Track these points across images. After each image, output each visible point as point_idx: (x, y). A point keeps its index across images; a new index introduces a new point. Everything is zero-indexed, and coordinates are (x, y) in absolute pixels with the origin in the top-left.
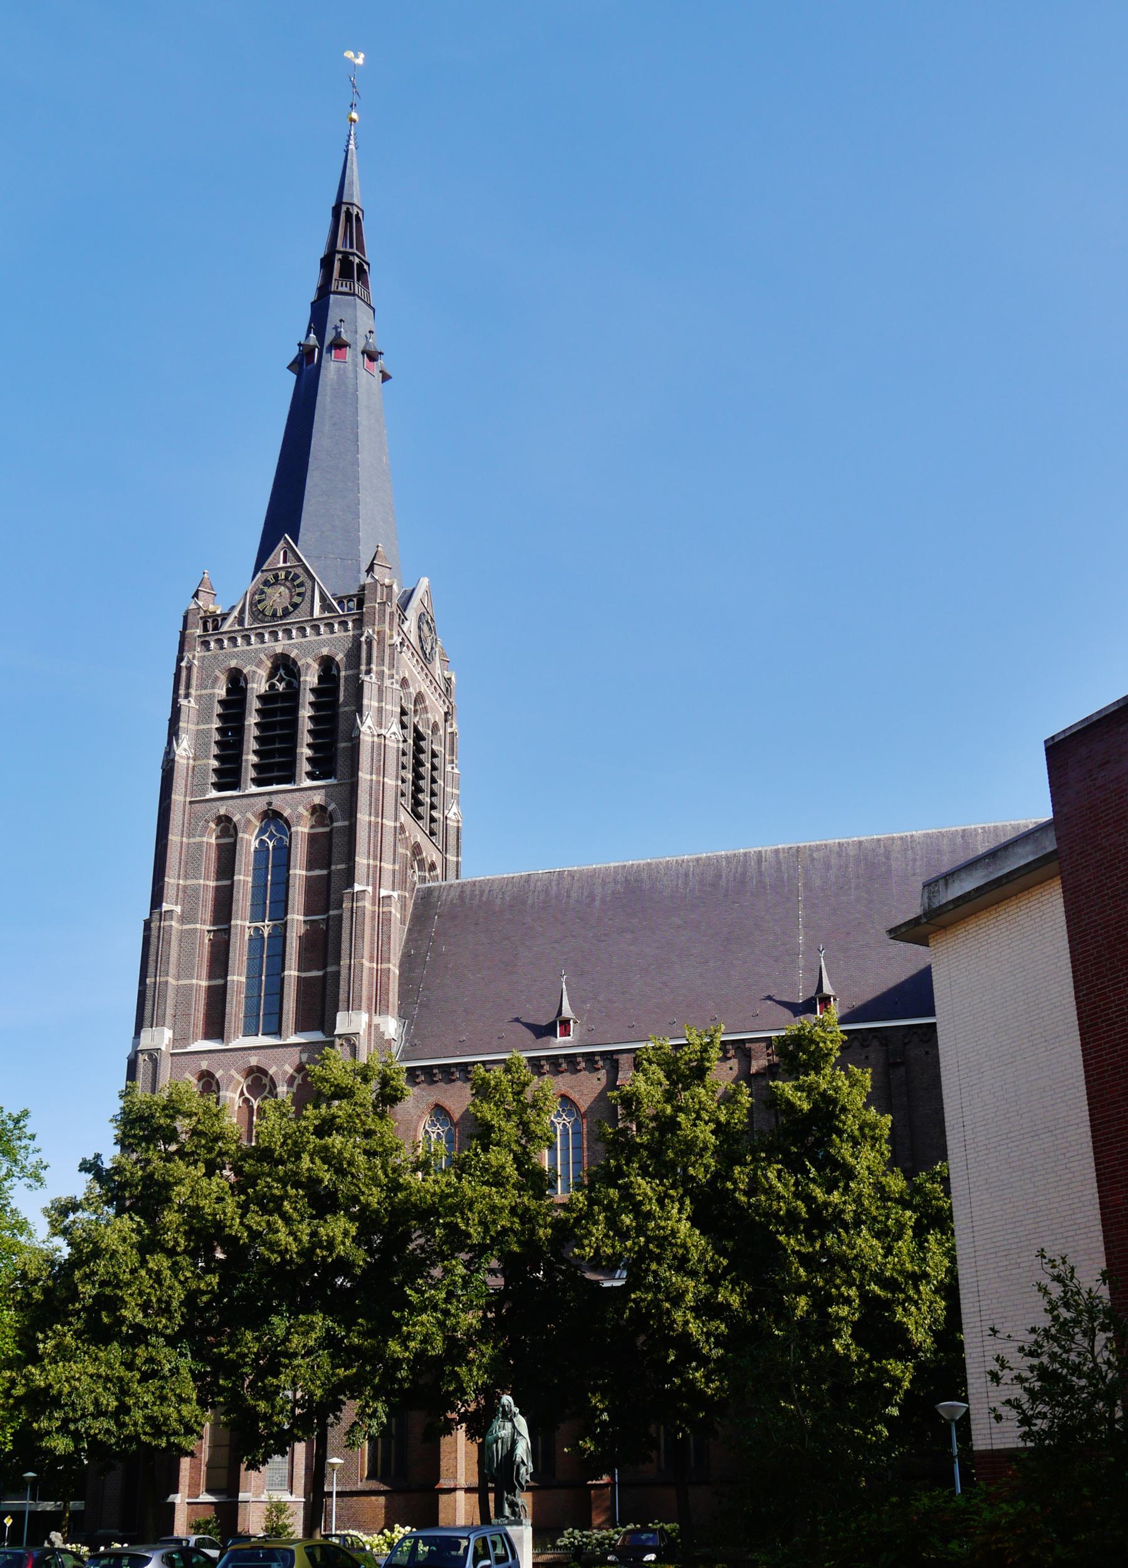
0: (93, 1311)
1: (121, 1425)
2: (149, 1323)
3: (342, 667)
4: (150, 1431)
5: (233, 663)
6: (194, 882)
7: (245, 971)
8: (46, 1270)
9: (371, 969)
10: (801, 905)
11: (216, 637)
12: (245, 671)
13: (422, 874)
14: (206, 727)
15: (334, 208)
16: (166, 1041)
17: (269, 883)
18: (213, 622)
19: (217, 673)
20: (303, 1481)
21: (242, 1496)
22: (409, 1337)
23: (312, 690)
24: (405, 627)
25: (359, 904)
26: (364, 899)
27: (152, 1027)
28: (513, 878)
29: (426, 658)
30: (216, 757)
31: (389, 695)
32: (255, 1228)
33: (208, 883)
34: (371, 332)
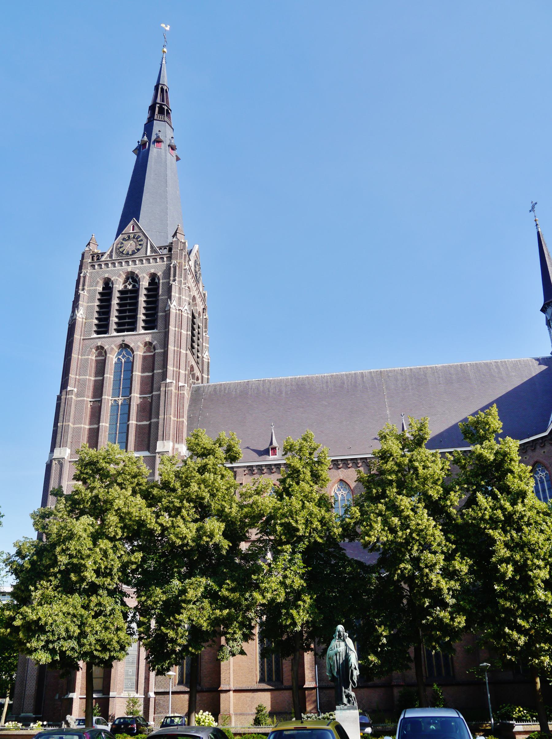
0: (65, 573)
1: (81, 645)
2: (98, 581)
3: (161, 278)
4: (100, 649)
5: (106, 276)
6: (84, 377)
7: (108, 421)
8: (32, 549)
9: (174, 421)
10: (386, 397)
11: (98, 263)
12: (112, 279)
13: (194, 381)
14: (92, 304)
15: (155, 86)
16: (67, 455)
17: (122, 379)
18: (97, 257)
19: (98, 279)
20: (143, 686)
21: (112, 694)
22: (266, 590)
23: (146, 289)
24: (190, 263)
25: (169, 389)
26: (171, 386)
27: (60, 447)
28: (240, 382)
29: (197, 281)
30: (96, 318)
31: (184, 292)
32: (164, 524)
33: (91, 378)
34: (172, 138)
